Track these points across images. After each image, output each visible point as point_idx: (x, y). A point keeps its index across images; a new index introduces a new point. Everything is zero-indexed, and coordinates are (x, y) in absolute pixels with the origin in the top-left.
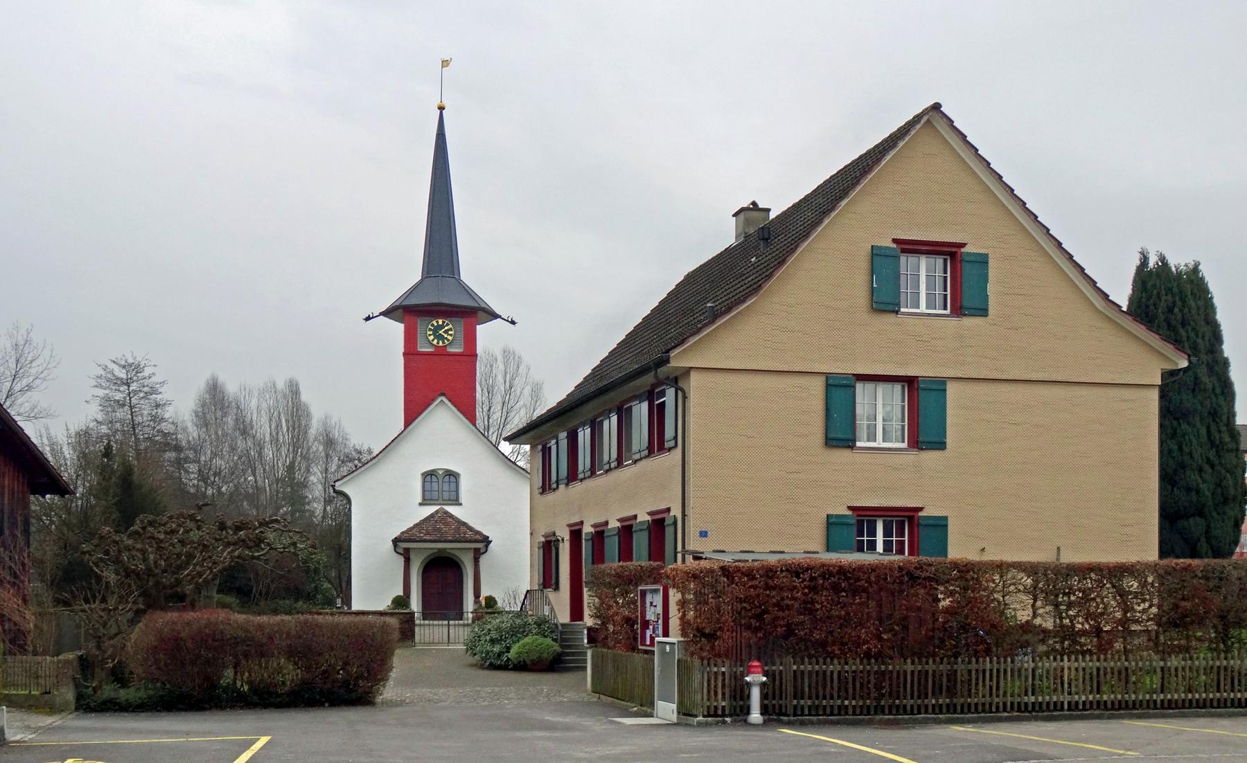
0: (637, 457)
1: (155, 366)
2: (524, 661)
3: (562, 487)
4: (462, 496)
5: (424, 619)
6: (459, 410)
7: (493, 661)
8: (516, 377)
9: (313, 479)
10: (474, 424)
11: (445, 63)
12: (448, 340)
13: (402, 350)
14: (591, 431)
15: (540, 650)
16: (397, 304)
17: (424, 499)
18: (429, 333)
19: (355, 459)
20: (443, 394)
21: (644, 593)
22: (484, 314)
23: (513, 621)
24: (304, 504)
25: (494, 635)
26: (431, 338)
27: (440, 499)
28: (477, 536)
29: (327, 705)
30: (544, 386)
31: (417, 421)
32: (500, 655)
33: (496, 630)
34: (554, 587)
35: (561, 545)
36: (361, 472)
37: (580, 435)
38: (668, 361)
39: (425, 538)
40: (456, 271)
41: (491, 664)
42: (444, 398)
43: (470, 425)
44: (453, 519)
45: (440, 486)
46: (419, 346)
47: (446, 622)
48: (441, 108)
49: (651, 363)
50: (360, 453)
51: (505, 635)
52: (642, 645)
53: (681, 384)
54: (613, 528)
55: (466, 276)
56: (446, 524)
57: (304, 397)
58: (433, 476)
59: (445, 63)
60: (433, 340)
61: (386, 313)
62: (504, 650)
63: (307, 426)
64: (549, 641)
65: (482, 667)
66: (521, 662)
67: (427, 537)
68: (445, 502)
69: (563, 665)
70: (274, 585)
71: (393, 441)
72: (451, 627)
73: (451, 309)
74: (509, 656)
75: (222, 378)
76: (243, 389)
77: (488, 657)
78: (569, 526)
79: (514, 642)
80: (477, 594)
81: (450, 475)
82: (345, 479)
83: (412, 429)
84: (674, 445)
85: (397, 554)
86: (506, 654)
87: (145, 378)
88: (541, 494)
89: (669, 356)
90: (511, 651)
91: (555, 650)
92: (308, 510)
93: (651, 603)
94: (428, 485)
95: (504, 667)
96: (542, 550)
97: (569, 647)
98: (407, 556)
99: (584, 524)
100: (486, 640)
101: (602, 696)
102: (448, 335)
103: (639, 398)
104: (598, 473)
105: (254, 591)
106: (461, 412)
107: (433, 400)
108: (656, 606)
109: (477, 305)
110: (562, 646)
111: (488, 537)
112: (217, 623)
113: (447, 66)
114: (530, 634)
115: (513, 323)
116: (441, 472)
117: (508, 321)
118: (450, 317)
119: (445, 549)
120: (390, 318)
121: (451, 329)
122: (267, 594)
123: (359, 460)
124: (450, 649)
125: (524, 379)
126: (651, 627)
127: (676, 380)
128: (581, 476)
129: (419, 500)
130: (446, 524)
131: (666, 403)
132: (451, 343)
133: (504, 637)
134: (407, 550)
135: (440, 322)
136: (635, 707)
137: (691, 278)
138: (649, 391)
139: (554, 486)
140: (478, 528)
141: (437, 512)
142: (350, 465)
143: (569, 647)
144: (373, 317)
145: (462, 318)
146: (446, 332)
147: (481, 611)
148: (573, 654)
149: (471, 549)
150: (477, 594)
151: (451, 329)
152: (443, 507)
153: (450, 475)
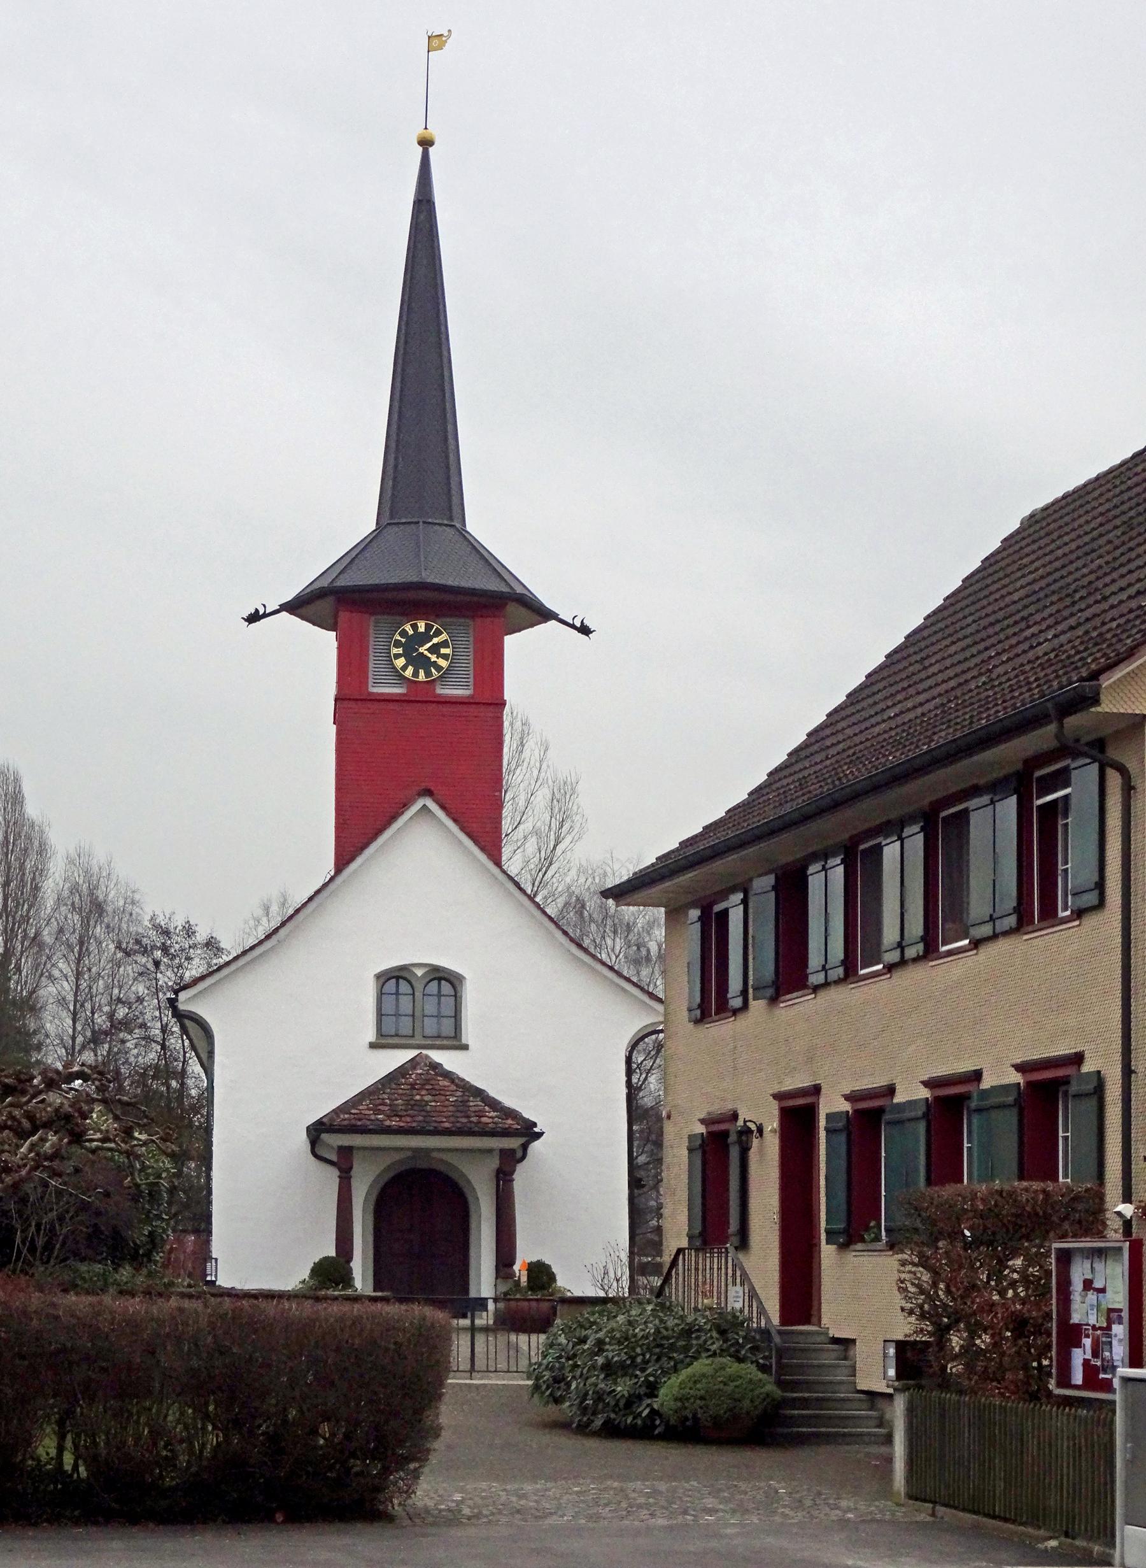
0: (986, 930)
2: (695, 1415)
3: (757, 1006)
4: (470, 1030)
6: (463, 829)
7: (613, 1416)
8: (517, 766)
9: (48, 992)
10: (498, 864)
11: (435, 42)
12: (439, 668)
14: (846, 872)
15: (733, 1391)
16: (325, 583)
17: (380, 1033)
18: (395, 651)
19: (154, 947)
20: (428, 793)
21: (1065, 1258)
22: (523, 611)
23: (661, 1321)
24: (27, 1051)
25: (613, 1353)
29: (279, 1517)
30: (579, 788)
31: (359, 861)
32: (631, 1401)
33: (619, 1343)
34: (735, 1240)
35: (755, 1142)
36: (227, 976)
37: (815, 882)
38: (1096, 701)
39: (388, 1123)
41: (607, 1423)
43: (490, 865)
44: (453, 1082)
48: (426, 143)
49: (1049, 705)
50: (166, 933)
51: (643, 1355)
52: (1060, 1385)
53: (1113, 753)
54: (910, 1102)
55: (475, 525)
56: (436, 1092)
57: (32, 810)
58: (401, 981)
59: (436, 42)
60: (404, 668)
61: (295, 607)
62: (643, 1390)
63: (40, 872)
64: (750, 1370)
65: (583, 1430)
66: (686, 1419)
67: (394, 1123)
69: (780, 1430)
70: (64, 1231)
73: (468, 599)
74: (656, 1406)
79: (665, 1373)
81: (440, 979)
82: (201, 986)
83: (355, 871)
84: (1096, 902)
85: (313, 1158)
86: (649, 1401)
88: (698, 1022)
89: (1100, 685)
90: (662, 1391)
91: (768, 1395)
92: (38, 1062)
93: (1088, 1285)
95: (643, 1432)
97: (794, 1386)
98: (343, 1163)
99: (823, 1091)
100: (594, 1367)
101: (941, 1510)
102: (439, 655)
103: (996, 788)
104: (862, 972)
105: (18, 1240)
106: (469, 835)
107: (405, 806)
108: (1103, 1291)
109: (505, 589)
110: (780, 1383)
112: (25, 1313)
113: (440, 47)
114: (704, 1355)
115: (585, 630)
116: (419, 972)
117: (573, 626)
118: (444, 616)
119: (427, 1152)
120: (303, 618)
121: (444, 644)
122: (48, 1247)
123: (165, 949)
125: (535, 772)
126: (1087, 1342)
127: (1100, 745)
128: (816, 979)
129: (371, 1035)
130: (436, 1092)
131: (1073, 802)
132: (445, 675)
133: (639, 1359)
134: (346, 1153)
136: (1051, 1538)
137: (1034, 521)
138: (1017, 774)
139: (736, 1003)
140: (508, 1102)
142: (143, 960)
143: (794, 1386)
144: (265, 615)
145: (473, 617)
146: (434, 649)
148: (805, 1403)
151: (444, 644)
152: (425, 1052)
153: (398, 978)
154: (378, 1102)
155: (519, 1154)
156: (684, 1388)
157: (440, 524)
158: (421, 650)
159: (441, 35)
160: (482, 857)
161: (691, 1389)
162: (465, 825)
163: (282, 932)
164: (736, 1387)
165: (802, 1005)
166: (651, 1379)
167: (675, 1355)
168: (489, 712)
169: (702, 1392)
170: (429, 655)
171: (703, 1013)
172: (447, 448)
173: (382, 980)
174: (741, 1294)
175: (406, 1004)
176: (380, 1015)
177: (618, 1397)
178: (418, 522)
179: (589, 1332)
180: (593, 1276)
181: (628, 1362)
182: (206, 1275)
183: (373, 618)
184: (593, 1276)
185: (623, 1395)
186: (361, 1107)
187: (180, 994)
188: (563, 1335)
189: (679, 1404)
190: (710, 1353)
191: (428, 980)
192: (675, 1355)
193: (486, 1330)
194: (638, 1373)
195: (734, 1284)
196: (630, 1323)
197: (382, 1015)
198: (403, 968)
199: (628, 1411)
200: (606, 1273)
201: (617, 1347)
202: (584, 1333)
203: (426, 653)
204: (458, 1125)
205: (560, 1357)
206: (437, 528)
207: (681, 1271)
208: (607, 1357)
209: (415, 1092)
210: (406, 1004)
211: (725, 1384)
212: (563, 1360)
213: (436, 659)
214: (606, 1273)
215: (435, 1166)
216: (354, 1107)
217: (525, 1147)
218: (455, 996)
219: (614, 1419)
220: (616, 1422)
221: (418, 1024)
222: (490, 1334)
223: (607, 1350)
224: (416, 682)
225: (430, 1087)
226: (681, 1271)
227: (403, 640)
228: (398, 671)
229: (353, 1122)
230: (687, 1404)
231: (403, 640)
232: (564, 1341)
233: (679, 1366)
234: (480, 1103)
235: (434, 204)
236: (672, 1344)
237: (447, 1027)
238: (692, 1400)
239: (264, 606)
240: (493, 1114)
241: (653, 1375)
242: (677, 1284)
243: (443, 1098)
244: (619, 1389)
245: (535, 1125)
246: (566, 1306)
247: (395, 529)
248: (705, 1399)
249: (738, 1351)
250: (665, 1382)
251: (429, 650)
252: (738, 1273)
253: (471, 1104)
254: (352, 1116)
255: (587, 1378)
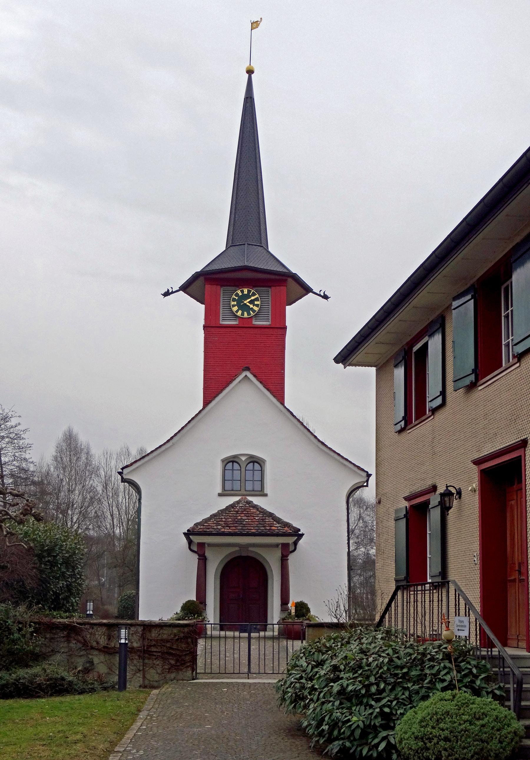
1: (20, 416)
4: (268, 481)
5: (222, 629)
7: (348, 744)
10: (283, 403)
11: (255, 25)
12: (254, 311)
13: (202, 322)
14: (475, 375)
18: (233, 303)
20: (248, 369)
26: (235, 309)
27: (243, 490)
28: (286, 529)
31: (218, 399)
33: (354, 670)
35: (455, 502)
39: (223, 530)
40: (263, 241)
42: (248, 374)
44: (258, 510)
45: (243, 474)
46: (221, 318)
47: (246, 635)
48: (250, 72)
51: (378, 685)
56: (248, 515)
58: (234, 463)
59: (255, 25)
60: (237, 311)
62: (378, 722)
67: (227, 530)
68: (248, 493)
71: (189, 422)
72: (252, 641)
74: (392, 741)
75: (76, 430)
76: (105, 454)
77: (336, 733)
78: (477, 462)
80: (284, 601)
81: (254, 462)
83: (212, 408)
86: (384, 734)
87: (12, 427)
94: (228, 474)
96: (403, 523)
107: (236, 376)
111: (299, 530)
114: (439, 686)
115: (326, 297)
116: (243, 459)
117: (320, 295)
121: (257, 299)
124: (250, 685)
129: (219, 490)
130: (248, 515)
133: (373, 689)
134: (201, 545)
135: (246, 291)
141: (238, 502)
144: (173, 292)
146: (252, 302)
147: (290, 620)
149: (277, 545)
150: (284, 601)
151: (257, 299)
154: (219, 520)
155: (291, 548)
156: (425, 727)
157: (255, 245)
158: (245, 302)
159: (258, 21)
160: (274, 400)
161: (433, 728)
162: (266, 384)
163: (175, 439)
164: (483, 726)
165: (502, 379)
166: (387, 710)
167: (409, 685)
168: (280, 332)
169: (446, 732)
170: (249, 305)
171: (406, 425)
172: (259, 211)
173: (226, 462)
174: (467, 624)
175: (237, 474)
176: (224, 480)
177: (353, 727)
178: (245, 244)
179: (325, 657)
180: (330, 609)
181: (363, 691)
182: (87, 611)
183: (222, 289)
184: (330, 609)
185: (358, 726)
186: (209, 523)
187: (124, 470)
188: (304, 658)
189: (420, 744)
190: (445, 684)
191: (248, 462)
192: (409, 685)
193: (273, 638)
194: (373, 703)
195: (457, 613)
196: (362, 651)
197: (225, 480)
198: (235, 456)
199: (364, 741)
200: (338, 606)
201: (351, 675)
202: (322, 657)
203: (248, 304)
204: (259, 531)
205: (301, 678)
206: (254, 246)
207: (400, 605)
208: (342, 686)
209: (238, 515)
210: (237, 474)
211: (471, 724)
212: (303, 681)
213: (252, 307)
214: (338, 606)
215: (250, 555)
216: (206, 522)
217: (295, 543)
218: (261, 470)
219: (350, 748)
220: (351, 751)
221: (243, 484)
222: (275, 641)
223: (342, 678)
224: (243, 318)
225: (246, 512)
226: (400, 605)
227: (237, 298)
228: (234, 314)
229: (205, 530)
230: (428, 745)
231: (237, 298)
232: (305, 664)
233: (415, 698)
234: (271, 520)
235: (254, 99)
236: (406, 674)
237: (258, 487)
238: (435, 740)
239: (172, 288)
240: (277, 525)
241: (389, 706)
242: (396, 614)
243: (253, 518)
244: (355, 719)
245: (299, 530)
246: (311, 630)
247: (234, 247)
248: (450, 741)
249: (473, 682)
250: (402, 714)
251: (249, 302)
252: (462, 602)
253: (267, 520)
254: (205, 527)
255: (323, 703)
